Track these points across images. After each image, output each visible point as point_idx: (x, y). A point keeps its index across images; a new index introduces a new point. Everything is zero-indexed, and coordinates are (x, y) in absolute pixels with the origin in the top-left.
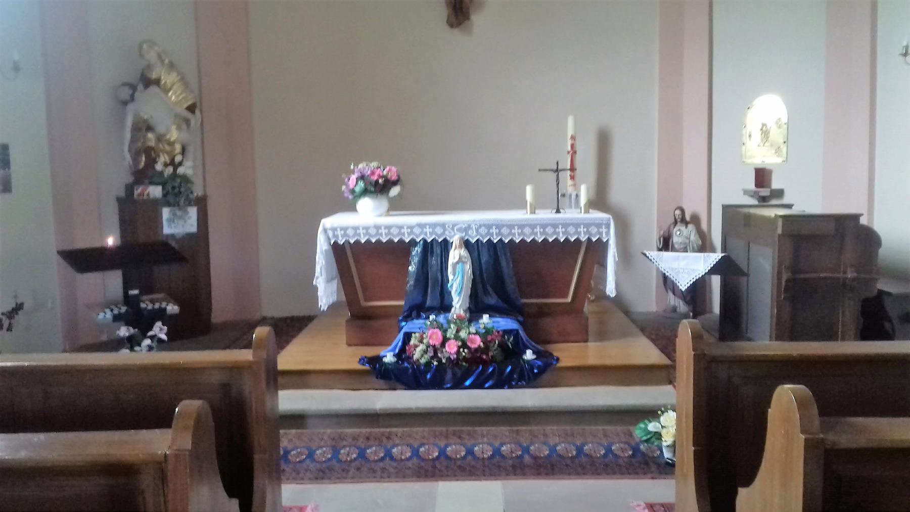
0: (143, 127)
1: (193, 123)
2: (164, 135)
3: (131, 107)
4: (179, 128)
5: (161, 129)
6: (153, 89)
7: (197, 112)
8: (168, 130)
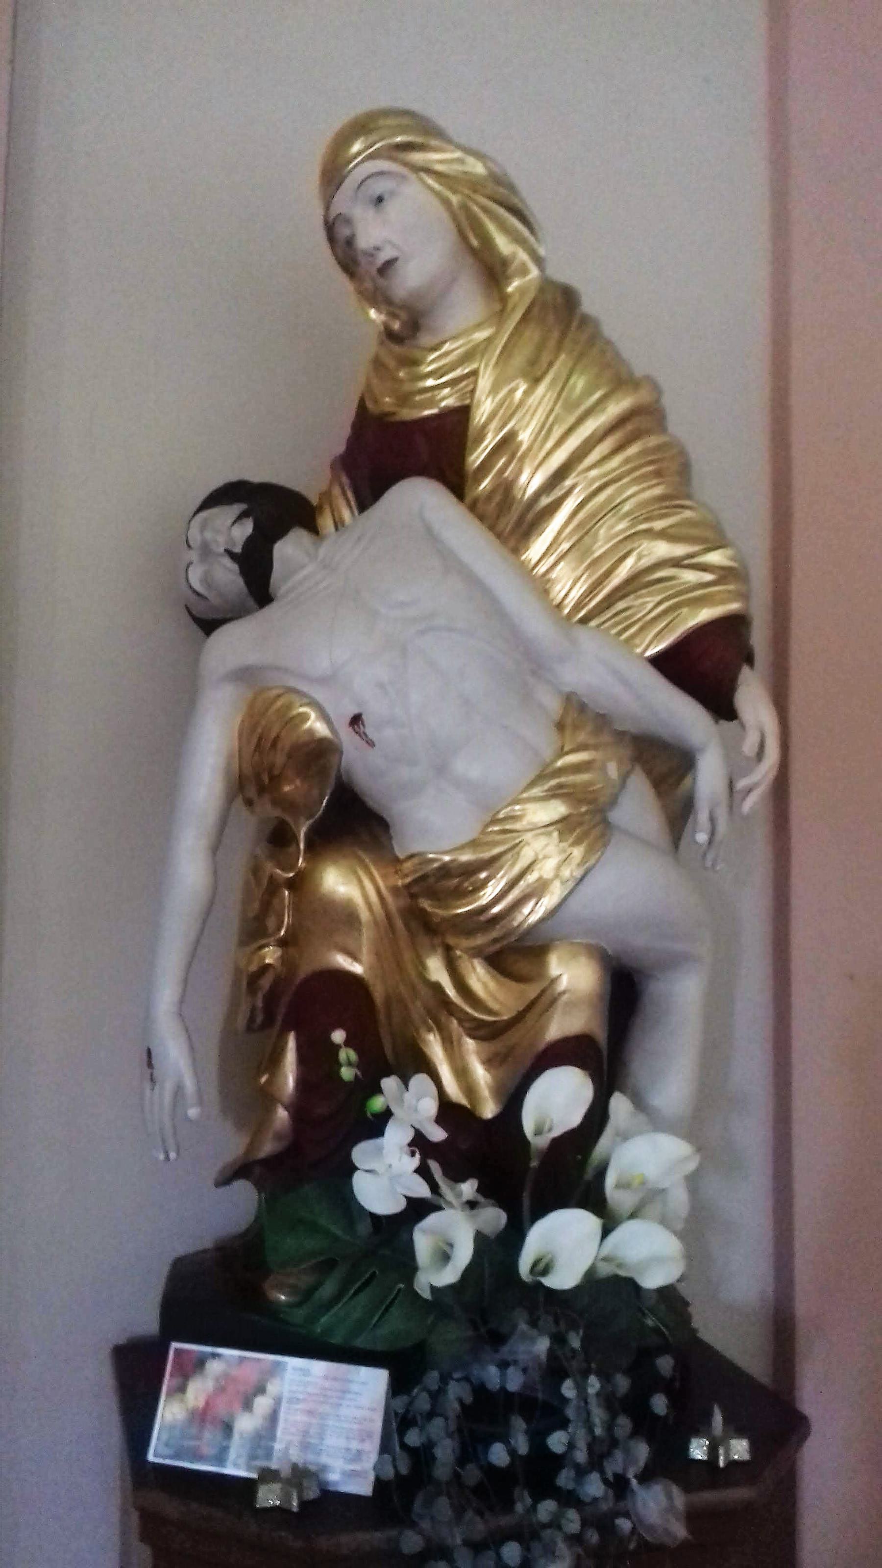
0: (312, 800)
1: (709, 777)
2: (459, 879)
3: (234, 645)
4: (589, 821)
5: (434, 829)
6: (419, 498)
7: (752, 696)
8: (498, 825)
